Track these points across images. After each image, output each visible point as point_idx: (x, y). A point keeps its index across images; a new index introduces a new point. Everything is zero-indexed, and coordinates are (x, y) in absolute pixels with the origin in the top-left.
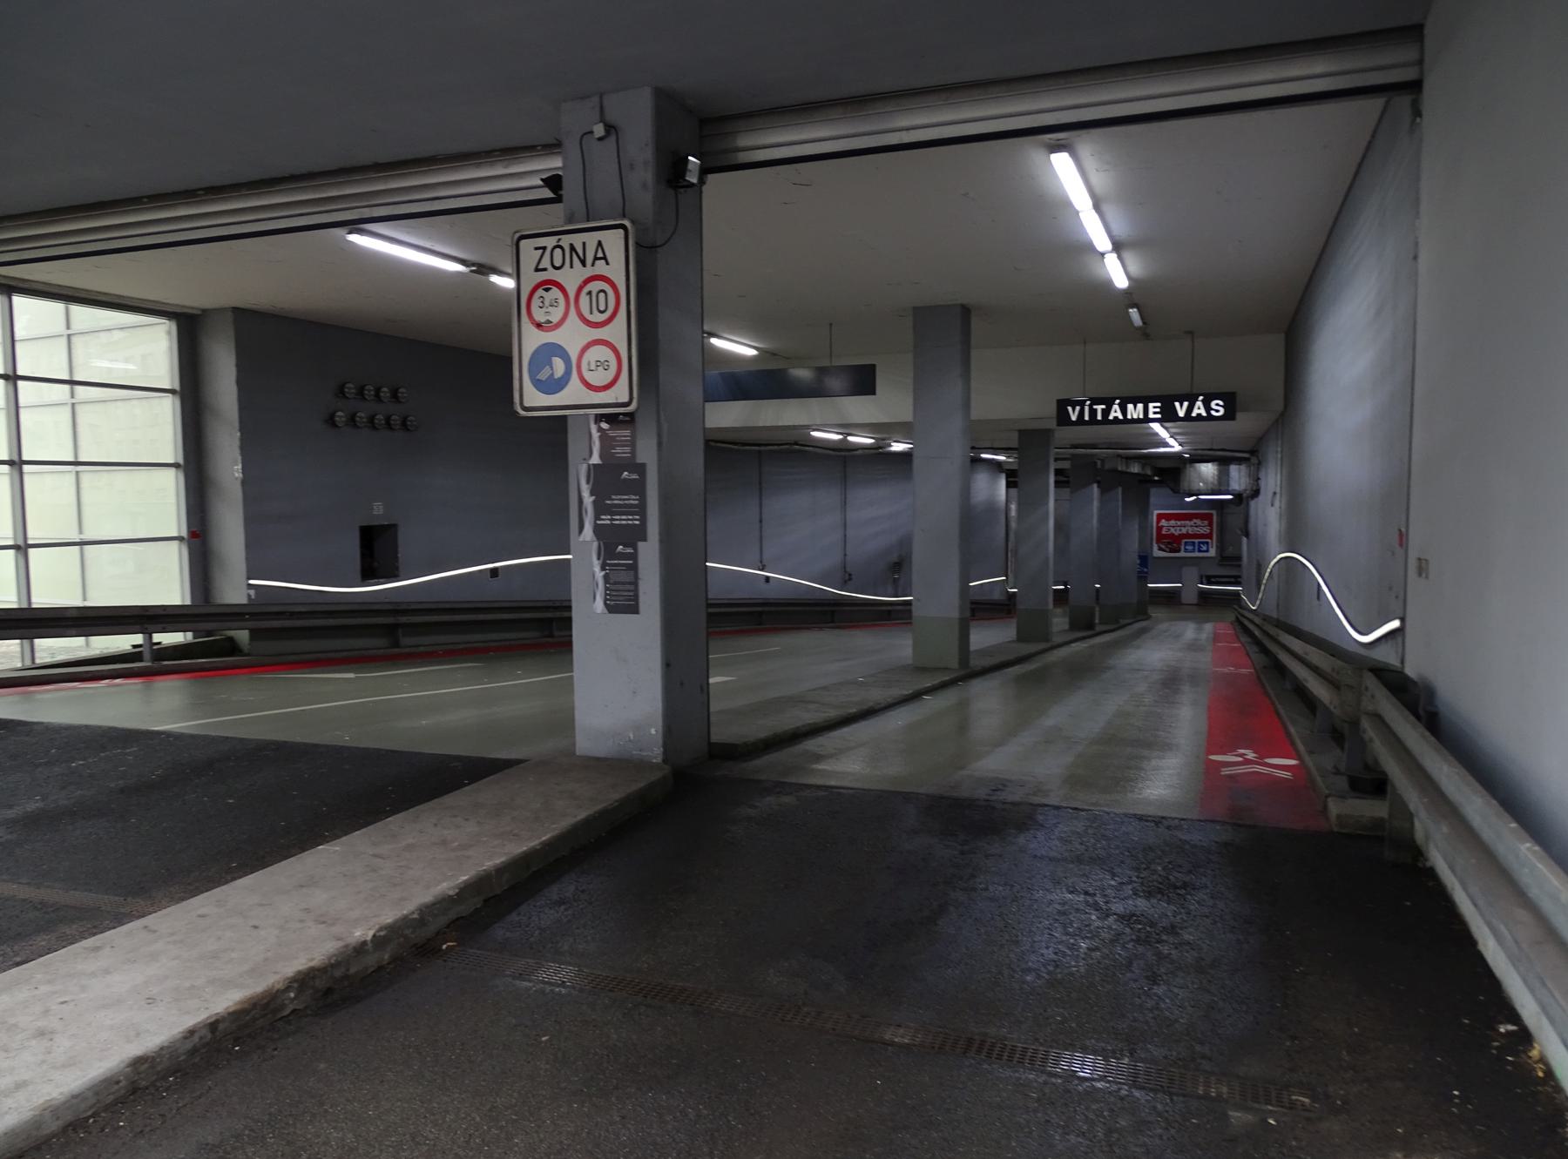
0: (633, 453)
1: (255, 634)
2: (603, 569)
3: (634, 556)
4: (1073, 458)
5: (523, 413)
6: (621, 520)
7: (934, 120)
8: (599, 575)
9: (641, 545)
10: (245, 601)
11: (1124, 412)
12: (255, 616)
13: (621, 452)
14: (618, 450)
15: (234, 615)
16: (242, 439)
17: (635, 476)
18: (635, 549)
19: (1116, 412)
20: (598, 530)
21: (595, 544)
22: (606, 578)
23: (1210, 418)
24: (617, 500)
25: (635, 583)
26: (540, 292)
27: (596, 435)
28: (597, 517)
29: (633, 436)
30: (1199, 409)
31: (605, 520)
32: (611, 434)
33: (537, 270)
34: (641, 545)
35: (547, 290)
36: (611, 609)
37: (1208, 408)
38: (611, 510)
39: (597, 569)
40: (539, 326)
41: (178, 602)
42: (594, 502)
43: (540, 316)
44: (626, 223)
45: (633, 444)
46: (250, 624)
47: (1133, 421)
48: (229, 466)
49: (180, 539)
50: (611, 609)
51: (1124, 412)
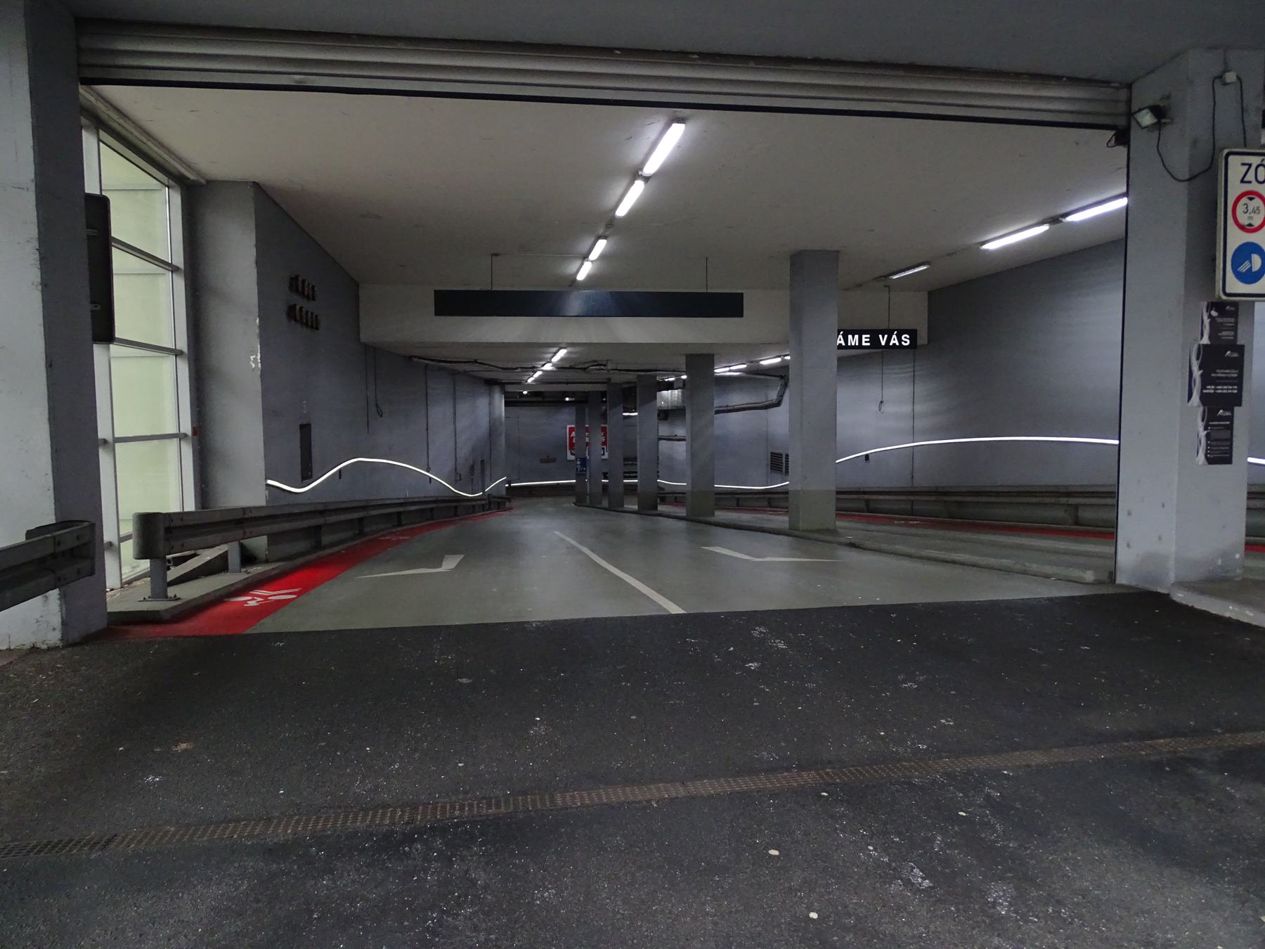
0: (1235, 336)
1: (274, 539)
2: (1206, 428)
3: (1231, 419)
4: (608, 382)
5: (1224, 298)
6: (1223, 389)
7: (774, 93)
8: (1203, 434)
9: (1236, 409)
10: (262, 502)
11: (846, 340)
12: (272, 518)
13: (1226, 334)
14: (1224, 333)
15: (242, 521)
16: (262, 327)
17: (1236, 355)
18: (1232, 412)
19: (894, 341)
20: (1204, 398)
21: (1201, 408)
22: (1208, 436)
23: (860, 346)
24: (1220, 373)
25: (1231, 440)
26: (1245, 200)
27: (1207, 321)
28: (1203, 387)
29: (1236, 323)
30: (894, 341)
31: (1210, 389)
32: (1220, 320)
33: (1242, 181)
34: (1236, 409)
35: (1251, 199)
36: (1211, 461)
37: (900, 340)
38: (1216, 381)
39: (1201, 429)
40: (1242, 227)
41: (174, 508)
42: (1202, 375)
43: (1243, 220)
44: (1226, 151)
45: (1235, 328)
46: (268, 528)
47: (852, 347)
48: (243, 351)
49: (181, 437)
50: (1211, 461)
51: (846, 340)
